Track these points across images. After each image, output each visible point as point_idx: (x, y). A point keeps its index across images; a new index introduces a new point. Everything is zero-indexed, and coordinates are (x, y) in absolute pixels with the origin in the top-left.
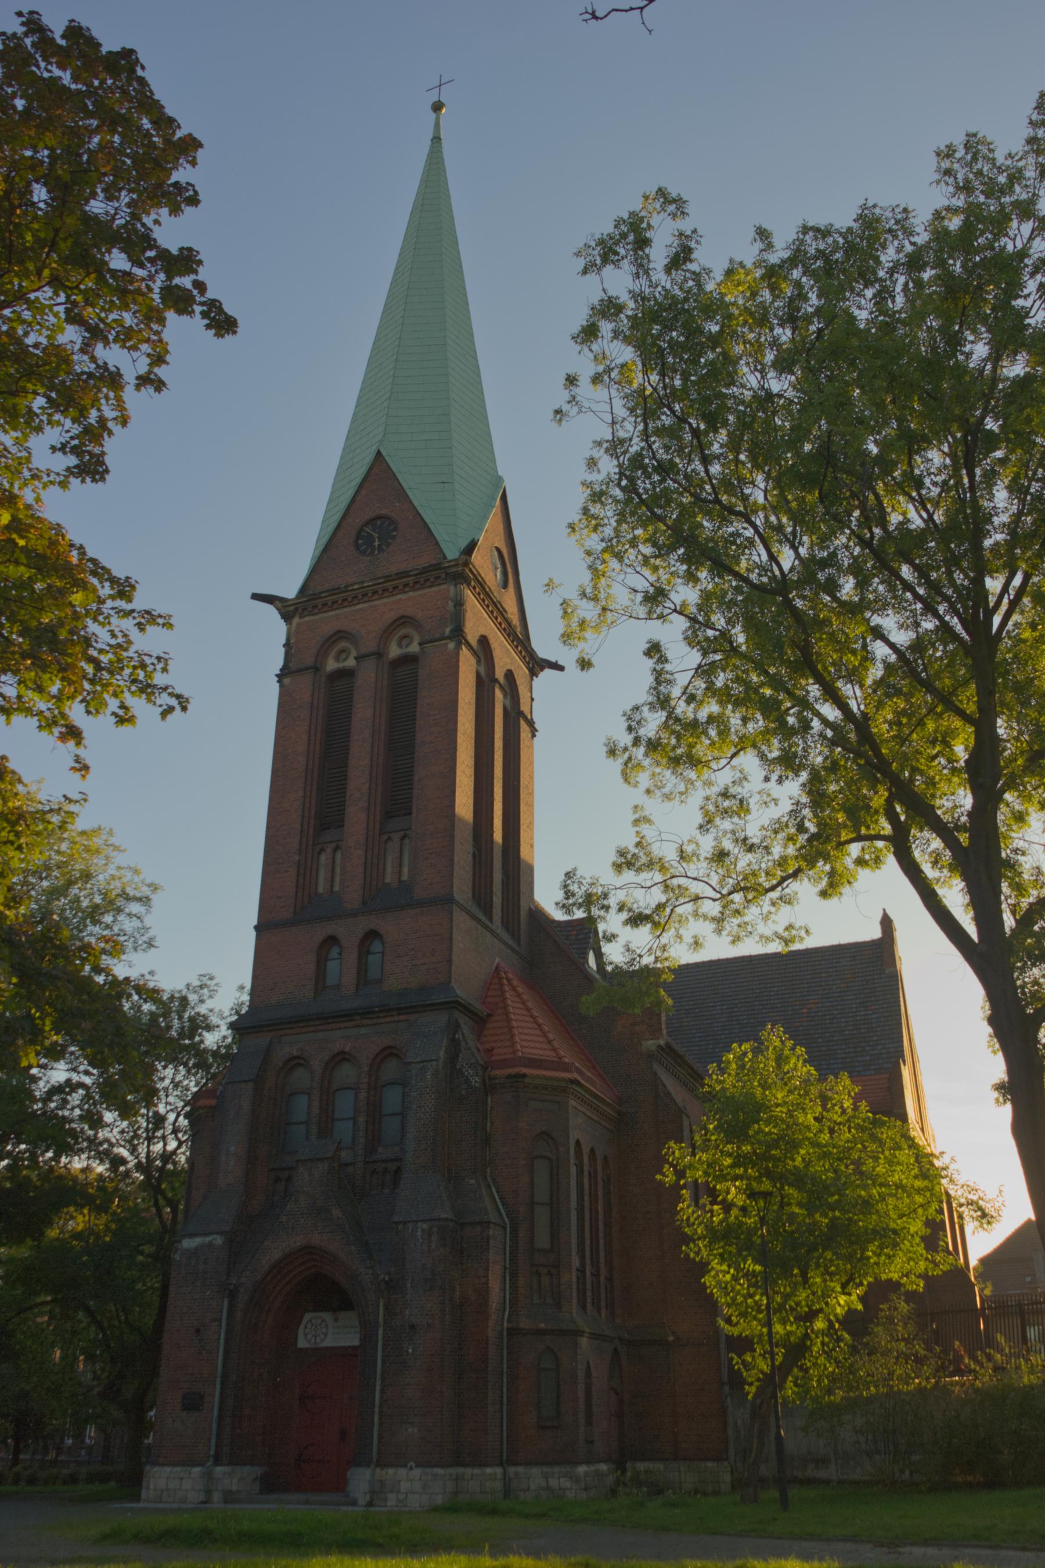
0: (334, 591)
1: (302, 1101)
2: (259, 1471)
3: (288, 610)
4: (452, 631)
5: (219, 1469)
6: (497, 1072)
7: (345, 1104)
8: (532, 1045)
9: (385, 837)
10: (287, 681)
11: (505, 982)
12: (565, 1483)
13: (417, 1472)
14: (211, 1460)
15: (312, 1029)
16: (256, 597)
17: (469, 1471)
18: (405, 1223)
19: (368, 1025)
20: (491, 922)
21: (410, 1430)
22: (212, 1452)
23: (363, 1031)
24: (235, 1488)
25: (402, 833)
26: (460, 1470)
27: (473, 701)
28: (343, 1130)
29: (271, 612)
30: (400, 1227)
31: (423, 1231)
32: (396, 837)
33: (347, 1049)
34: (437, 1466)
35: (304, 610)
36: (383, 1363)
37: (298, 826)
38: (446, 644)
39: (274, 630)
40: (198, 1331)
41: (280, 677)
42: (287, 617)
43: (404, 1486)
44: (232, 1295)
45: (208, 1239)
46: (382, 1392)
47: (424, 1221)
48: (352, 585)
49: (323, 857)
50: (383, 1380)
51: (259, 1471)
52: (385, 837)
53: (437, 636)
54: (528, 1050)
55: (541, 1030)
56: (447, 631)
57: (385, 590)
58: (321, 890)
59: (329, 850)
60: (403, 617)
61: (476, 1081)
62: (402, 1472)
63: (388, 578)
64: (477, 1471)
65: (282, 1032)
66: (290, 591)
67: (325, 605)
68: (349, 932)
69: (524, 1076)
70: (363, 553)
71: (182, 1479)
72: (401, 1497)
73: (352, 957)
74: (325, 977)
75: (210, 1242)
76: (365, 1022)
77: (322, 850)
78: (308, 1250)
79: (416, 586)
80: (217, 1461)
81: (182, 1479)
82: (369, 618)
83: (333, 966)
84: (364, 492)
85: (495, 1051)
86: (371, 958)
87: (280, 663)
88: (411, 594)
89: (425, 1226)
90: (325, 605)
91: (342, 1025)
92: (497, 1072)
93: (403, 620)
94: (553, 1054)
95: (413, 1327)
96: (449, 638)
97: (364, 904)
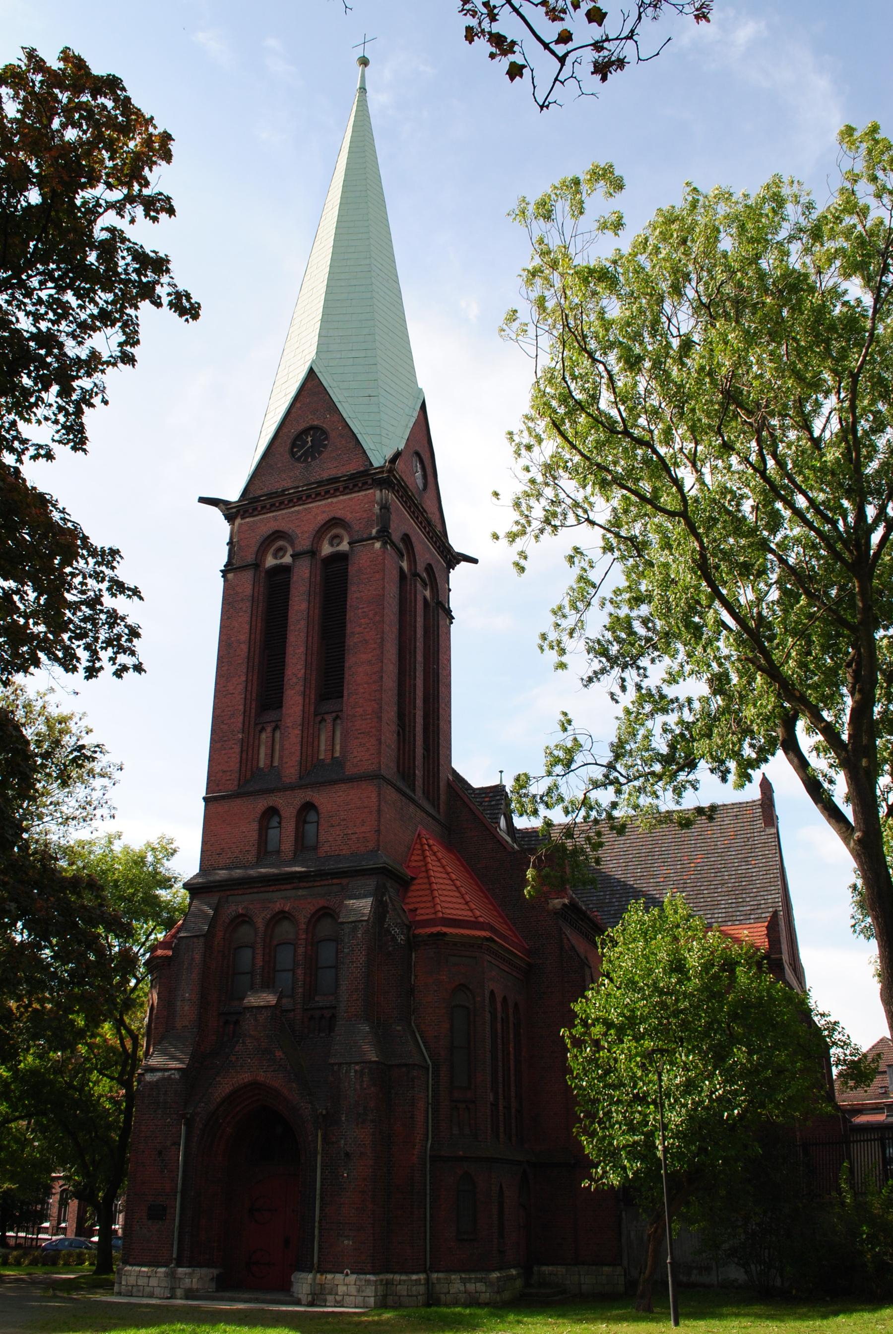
0: (270, 495)
2: (215, 1272)
3: (231, 511)
4: (378, 532)
5: (180, 1270)
8: (451, 906)
9: (319, 718)
10: (230, 576)
11: (427, 847)
12: (481, 1287)
13: (353, 1277)
14: (174, 1262)
15: (255, 890)
16: (203, 500)
17: (397, 1277)
18: (340, 1064)
19: (305, 888)
21: (346, 1242)
22: (174, 1256)
23: (301, 892)
24: (195, 1286)
25: (334, 715)
29: (216, 513)
30: (336, 1068)
31: (356, 1071)
32: (329, 718)
33: (287, 909)
34: (370, 1274)
35: (245, 512)
36: (322, 1185)
37: (241, 707)
38: (373, 543)
40: (160, 1153)
41: (225, 573)
42: (230, 518)
43: (342, 1289)
44: (189, 1124)
45: (166, 1074)
46: (321, 1210)
47: (356, 1063)
48: (288, 490)
50: (322, 1199)
51: (215, 1272)
52: (319, 718)
53: (365, 536)
56: (374, 531)
57: (318, 494)
59: (269, 729)
60: (334, 518)
61: (401, 939)
62: (339, 1277)
63: (320, 483)
64: (404, 1277)
65: (228, 893)
66: (233, 494)
67: (263, 507)
69: (445, 934)
70: (298, 460)
71: (149, 1277)
72: (339, 1298)
73: (289, 826)
74: (266, 843)
75: (169, 1076)
77: (263, 729)
79: (346, 490)
80: (179, 1265)
81: (149, 1277)
82: (303, 520)
84: (298, 405)
85: (418, 912)
87: (224, 559)
88: (341, 498)
89: (357, 1067)
90: (263, 507)
91: (283, 887)
93: (335, 522)
94: (470, 914)
95: (347, 1155)
96: (376, 538)
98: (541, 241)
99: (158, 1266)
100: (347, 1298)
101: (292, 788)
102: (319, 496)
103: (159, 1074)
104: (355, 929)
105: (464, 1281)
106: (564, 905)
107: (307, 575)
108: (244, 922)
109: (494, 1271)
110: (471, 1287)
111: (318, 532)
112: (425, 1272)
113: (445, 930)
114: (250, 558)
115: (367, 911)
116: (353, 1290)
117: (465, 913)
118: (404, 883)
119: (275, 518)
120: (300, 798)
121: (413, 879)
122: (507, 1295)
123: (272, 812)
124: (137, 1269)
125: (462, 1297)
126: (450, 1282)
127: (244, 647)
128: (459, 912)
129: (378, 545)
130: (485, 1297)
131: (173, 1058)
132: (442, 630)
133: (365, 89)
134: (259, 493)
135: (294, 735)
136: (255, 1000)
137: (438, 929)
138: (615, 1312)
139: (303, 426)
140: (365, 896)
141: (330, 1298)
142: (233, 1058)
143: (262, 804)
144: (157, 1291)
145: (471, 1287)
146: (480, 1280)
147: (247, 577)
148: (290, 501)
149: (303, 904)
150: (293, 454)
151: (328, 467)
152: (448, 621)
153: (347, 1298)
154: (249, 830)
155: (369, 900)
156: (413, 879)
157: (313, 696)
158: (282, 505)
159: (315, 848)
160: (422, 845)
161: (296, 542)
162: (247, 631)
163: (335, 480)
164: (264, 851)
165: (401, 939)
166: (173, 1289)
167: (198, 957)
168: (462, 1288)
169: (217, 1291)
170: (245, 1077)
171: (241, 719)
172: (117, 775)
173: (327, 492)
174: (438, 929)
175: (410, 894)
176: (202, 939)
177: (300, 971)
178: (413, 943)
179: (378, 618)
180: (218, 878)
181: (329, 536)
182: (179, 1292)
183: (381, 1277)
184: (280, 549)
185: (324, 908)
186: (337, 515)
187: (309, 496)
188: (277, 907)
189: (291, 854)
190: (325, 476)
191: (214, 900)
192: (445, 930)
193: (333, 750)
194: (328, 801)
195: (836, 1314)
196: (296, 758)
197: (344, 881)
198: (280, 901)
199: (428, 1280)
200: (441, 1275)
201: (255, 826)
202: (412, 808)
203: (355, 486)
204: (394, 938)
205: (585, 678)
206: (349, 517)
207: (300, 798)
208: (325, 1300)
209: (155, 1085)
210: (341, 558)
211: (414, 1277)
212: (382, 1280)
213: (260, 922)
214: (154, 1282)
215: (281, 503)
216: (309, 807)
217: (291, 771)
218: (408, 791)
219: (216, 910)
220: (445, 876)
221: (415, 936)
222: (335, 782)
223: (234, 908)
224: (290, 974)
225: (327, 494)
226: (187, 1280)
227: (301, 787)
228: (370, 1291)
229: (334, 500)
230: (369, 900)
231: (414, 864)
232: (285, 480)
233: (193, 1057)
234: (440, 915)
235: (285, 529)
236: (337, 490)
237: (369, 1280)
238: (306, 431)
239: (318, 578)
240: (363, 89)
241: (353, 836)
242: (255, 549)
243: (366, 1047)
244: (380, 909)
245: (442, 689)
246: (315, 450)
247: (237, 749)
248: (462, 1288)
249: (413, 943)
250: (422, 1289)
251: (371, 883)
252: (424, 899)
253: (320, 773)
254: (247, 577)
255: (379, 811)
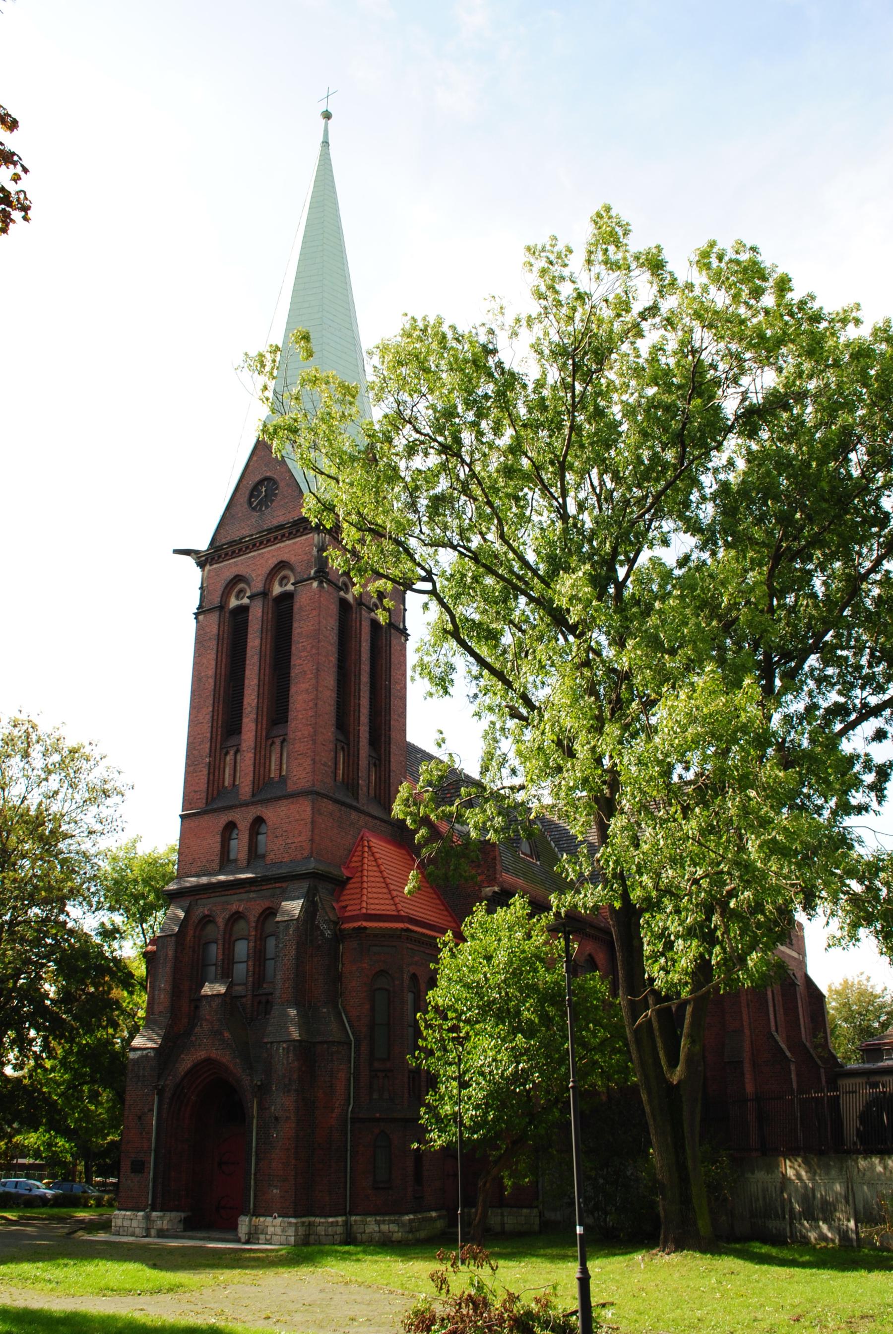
0: (231, 543)
1: (213, 948)
2: (183, 1215)
3: (203, 560)
4: (316, 572)
5: (154, 1214)
6: (346, 926)
7: (242, 949)
8: (377, 901)
9: (270, 741)
10: (201, 617)
11: (366, 849)
12: (394, 1228)
16: (176, 552)
17: (318, 1220)
18: (272, 1043)
20: (357, 799)
23: (252, 895)
24: (165, 1227)
26: (312, 1219)
27: (336, 628)
28: (240, 970)
29: (190, 561)
32: (278, 741)
33: (241, 909)
35: (213, 559)
36: (257, 1144)
37: (209, 735)
39: (191, 576)
40: (140, 1118)
41: (197, 615)
42: (201, 565)
43: (270, 1230)
44: (161, 1093)
46: (257, 1164)
47: (284, 1042)
49: (228, 758)
50: (257, 1155)
51: (183, 1215)
52: (270, 741)
54: (372, 907)
55: (388, 888)
56: (312, 572)
57: (268, 541)
58: (226, 784)
59: (232, 752)
60: (282, 562)
61: (328, 933)
62: (269, 1219)
63: (270, 531)
64: (322, 1220)
66: (202, 544)
67: (226, 554)
68: (243, 819)
69: (365, 928)
70: (254, 509)
72: (268, 1237)
73: (245, 837)
74: (228, 852)
76: (253, 888)
77: (227, 753)
78: (208, 1061)
80: (154, 1209)
82: (256, 565)
83: (233, 843)
84: (255, 458)
85: (349, 908)
86: (260, 837)
87: (197, 603)
90: (226, 554)
92: (346, 926)
93: (282, 565)
94: (393, 908)
95: (276, 1118)
96: (313, 578)
97: (253, 795)
98: (310, 354)
99: (139, 1211)
100: (274, 1237)
101: (246, 804)
102: (269, 542)
103: (139, 1053)
104: (287, 927)
105: (378, 1223)
106: (495, 892)
107: (260, 614)
108: (210, 921)
109: (407, 1214)
110: (385, 1228)
111: (269, 574)
112: (345, 1215)
113: (365, 924)
114: (216, 601)
115: (297, 912)
116: (279, 1230)
117: (388, 907)
118: (340, 884)
119: (236, 564)
120: (253, 812)
121: (349, 879)
122: (422, 1234)
123: (231, 826)
124: (123, 1213)
125: (377, 1236)
126: (365, 1223)
127: (211, 681)
128: (383, 907)
129: (315, 584)
130: (397, 1236)
131: (150, 1039)
132: (395, 647)
133: (327, 143)
134: (224, 541)
135: (247, 760)
136: (207, 989)
137: (359, 924)
138: (549, 1251)
139: (258, 478)
140: (298, 898)
141: (262, 1237)
142: (193, 1039)
143: (223, 819)
144: (137, 1231)
145: (385, 1228)
146: (393, 1222)
147: (214, 617)
148: (247, 548)
149: (251, 905)
150: (250, 503)
151: (277, 516)
152: (403, 639)
153: (274, 1237)
154: (214, 843)
155: (301, 902)
156: (349, 879)
157: (264, 722)
158: (240, 552)
159: (263, 856)
160: (363, 847)
161: (252, 584)
162: (214, 666)
163: (280, 527)
164: (225, 862)
165: (328, 933)
166: (148, 1230)
167: (171, 953)
168: (377, 1229)
169: (185, 1230)
170: (202, 1054)
171: (208, 745)
172: (128, 793)
173: (276, 538)
174: (359, 924)
175: (346, 892)
176: (173, 938)
177: (250, 963)
178: (340, 936)
179: (314, 651)
180: (188, 885)
181: (234, 593)
182: (153, 1232)
183: (304, 1219)
184: (284, 578)
185: (269, 908)
186: (284, 559)
187: (261, 543)
188: (234, 908)
189: (245, 863)
190: (275, 523)
191: (186, 903)
192: (365, 924)
193: (281, 769)
194: (274, 814)
195: (614, 1255)
196: (250, 778)
197: (284, 885)
198: (236, 903)
199: (346, 1223)
200: (358, 1218)
201: (218, 838)
202: (354, 815)
203: (298, 531)
204: (322, 934)
205: (471, 695)
206: (293, 560)
207: (253, 812)
208: (258, 1239)
209: (136, 1062)
210: (288, 597)
211: (331, 1220)
212: (303, 1223)
213: (221, 921)
214: (135, 1224)
215: (240, 550)
216: (259, 821)
217: (245, 789)
218: (348, 801)
219: (187, 913)
220: (378, 874)
221: (340, 930)
222: (279, 798)
223: (202, 910)
224: (245, 965)
225: (276, 540)
226: (159, 1223)
227: (253, 803)
228: (291, 1231)
229: (282, 545)
230: (301, 902)
231: (353, 865)
232: (242, 530)
233: (165, 1038)
234: (364, 911)
235: (244, 573)
236: (283, 536)
237: (290, 1223)
238: (261, 482)
239: (270, 616)
240: (326, 143)
241: (293, 846)
242: (220, 592)
243: (292, 1029)
244: (310, 910)
245: (394, 702)
246: (270, 497)
247: (206, 772)
248: (377, 1229)
249: (340, 936)
250: (339, 1230)
251: (304, 886)
252: (354, 897)
253: (268, 789)
254: (214, 617)
255: (313, 822)
